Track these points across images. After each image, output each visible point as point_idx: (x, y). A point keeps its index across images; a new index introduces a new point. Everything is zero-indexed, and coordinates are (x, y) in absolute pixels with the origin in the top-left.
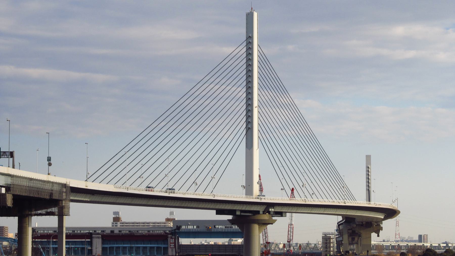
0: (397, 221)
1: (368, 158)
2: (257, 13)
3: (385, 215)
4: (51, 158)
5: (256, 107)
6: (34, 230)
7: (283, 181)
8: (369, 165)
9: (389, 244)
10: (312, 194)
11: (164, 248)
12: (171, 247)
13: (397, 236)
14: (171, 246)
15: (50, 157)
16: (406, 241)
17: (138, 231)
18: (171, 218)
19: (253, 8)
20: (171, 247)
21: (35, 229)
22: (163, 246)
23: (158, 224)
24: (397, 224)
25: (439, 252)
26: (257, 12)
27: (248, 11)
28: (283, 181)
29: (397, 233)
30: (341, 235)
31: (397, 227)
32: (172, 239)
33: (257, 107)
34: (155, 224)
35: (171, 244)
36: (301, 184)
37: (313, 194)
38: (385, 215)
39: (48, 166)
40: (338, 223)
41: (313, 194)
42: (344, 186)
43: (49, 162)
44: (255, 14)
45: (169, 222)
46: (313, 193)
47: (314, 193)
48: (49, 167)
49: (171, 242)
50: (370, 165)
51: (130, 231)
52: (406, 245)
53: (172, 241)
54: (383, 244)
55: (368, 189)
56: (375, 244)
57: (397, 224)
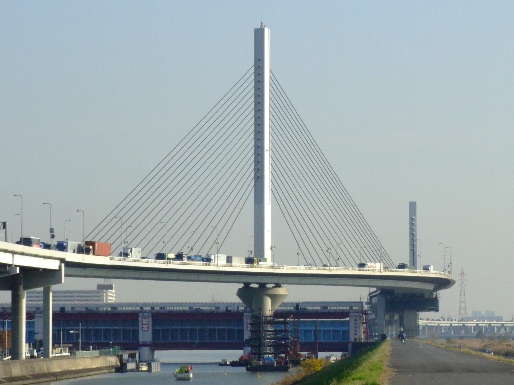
0: (462, 287)
1: (413, 206)
2: (269, 29)
3: (435, 286)
4: (54, 229)
5: (267, 151)
6: (5, 309)
7: (301, 243)
8: (413, 216)
9: (425, 324)
10: (337, 259)
11: (133, 330)
12: (144, 329)
13: (463, 312)
14: (147, 327)
15: (53, 229)
16: (489, 319)
17: (97, 308)
18: (106, 284)
19: (263, 23)
20: (144, 329)
21: (6, 309)
22: (132, 328)
23: (71, 293)
24: (462, 292)
25: (163, 311)
26: (268, 28)
27: (258, 27)
28: (301, 243)
29: (463, 306)
30: (373, 311)
31: (463, 296)
32: (145, 319)
33: (269, 150)
34: (66, 293)
35: (144, 326)
36: (325, 249)
37: (338, 259)
38: (435, 286)
39: (50, 238)
40: (370, 294)
41: (338, 259)
42: (381, 250)
43: (52, 234)
44: (266, 31)
45: (105, 291)
46: (339, 257)
47: (340, 258)
48: (52, 239)
49: (144, 323)
50: (415, 215)
51: (86, 308)
52: (475, 325)
53: (145, 322)
54: (439, 324)
55: (412, 243)
56: (426, 324)
57: (462, 292)
